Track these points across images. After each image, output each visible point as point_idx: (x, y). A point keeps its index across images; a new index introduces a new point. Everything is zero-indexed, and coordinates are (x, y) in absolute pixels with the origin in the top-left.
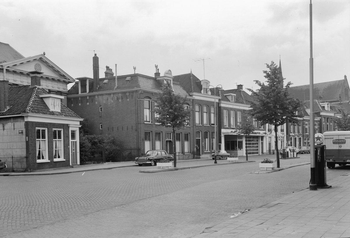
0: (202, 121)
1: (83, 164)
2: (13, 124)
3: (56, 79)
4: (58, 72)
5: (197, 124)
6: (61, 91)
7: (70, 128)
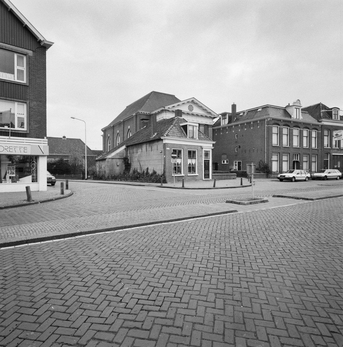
0: (339, 142)
1: (14, 73)
2: (240, 178)
3: (204, 115)
5: (325, 147)
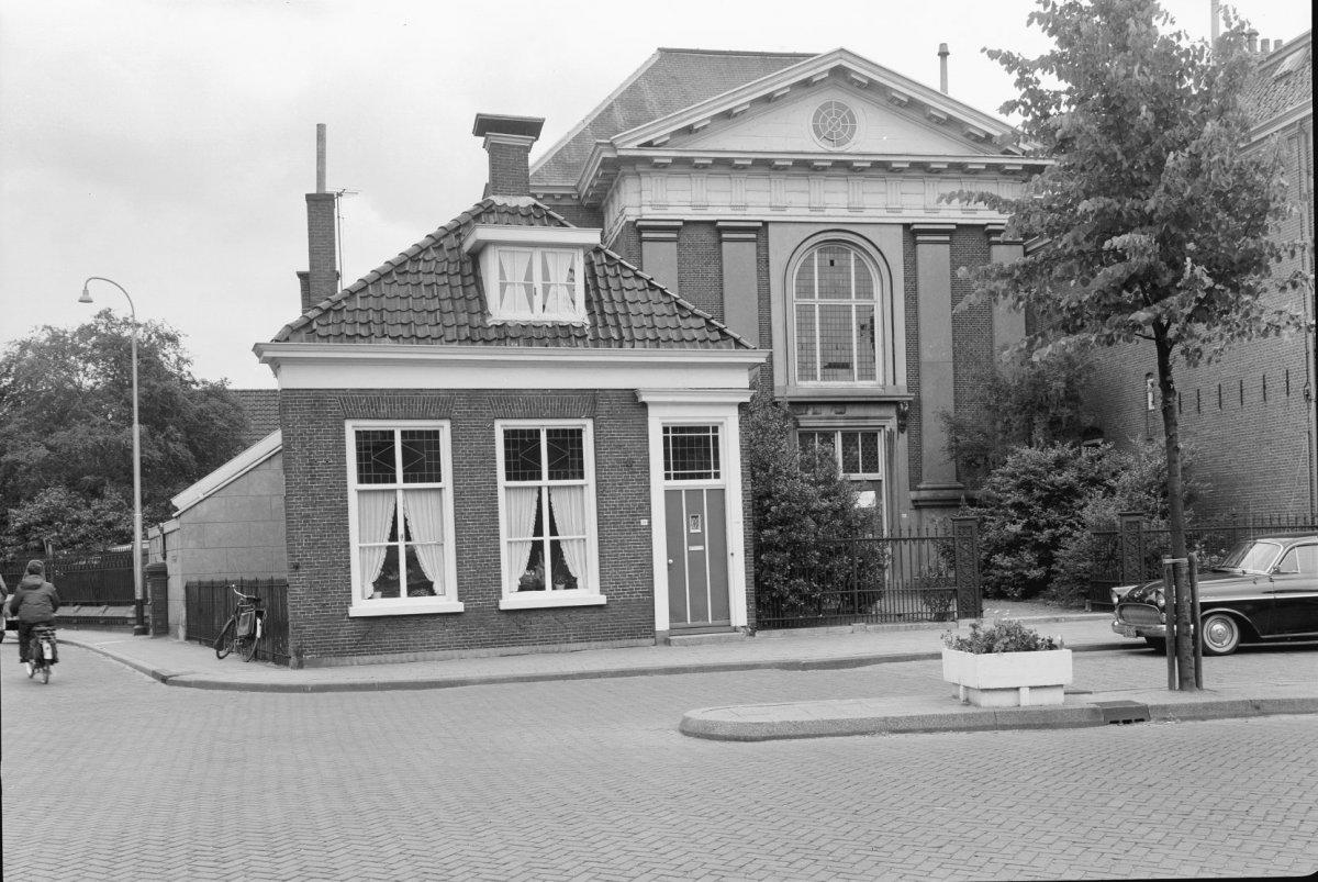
4: (950, 121)
6: (985, 222)
7: (652, 411)
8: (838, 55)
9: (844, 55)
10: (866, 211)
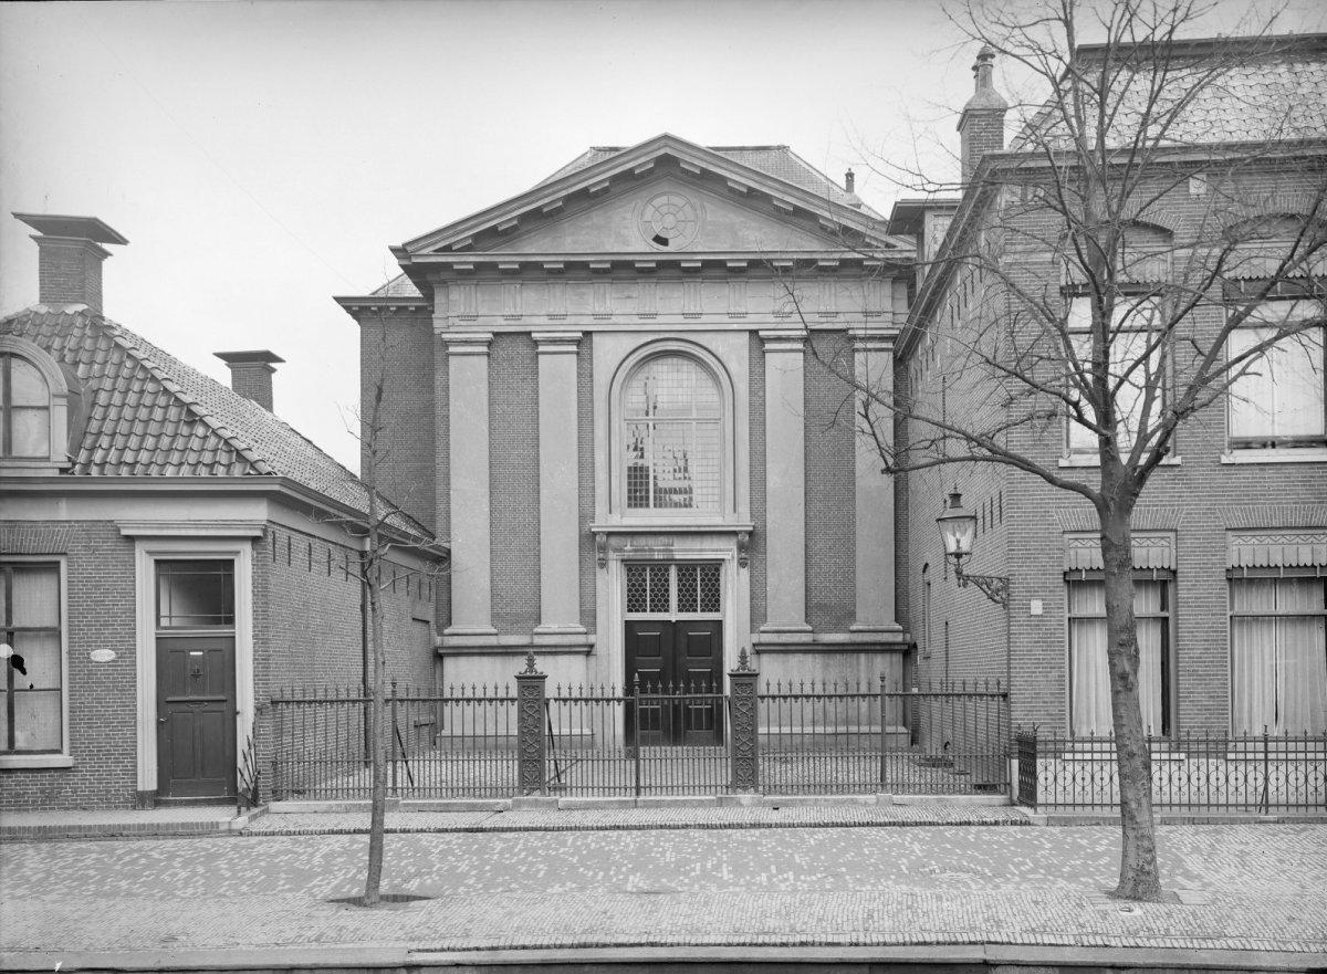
8: (663, 141)
9: (671, 143)
10: (480, 319)
